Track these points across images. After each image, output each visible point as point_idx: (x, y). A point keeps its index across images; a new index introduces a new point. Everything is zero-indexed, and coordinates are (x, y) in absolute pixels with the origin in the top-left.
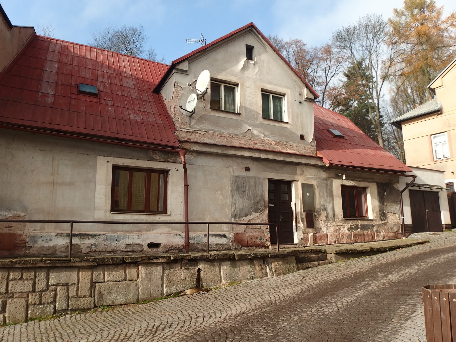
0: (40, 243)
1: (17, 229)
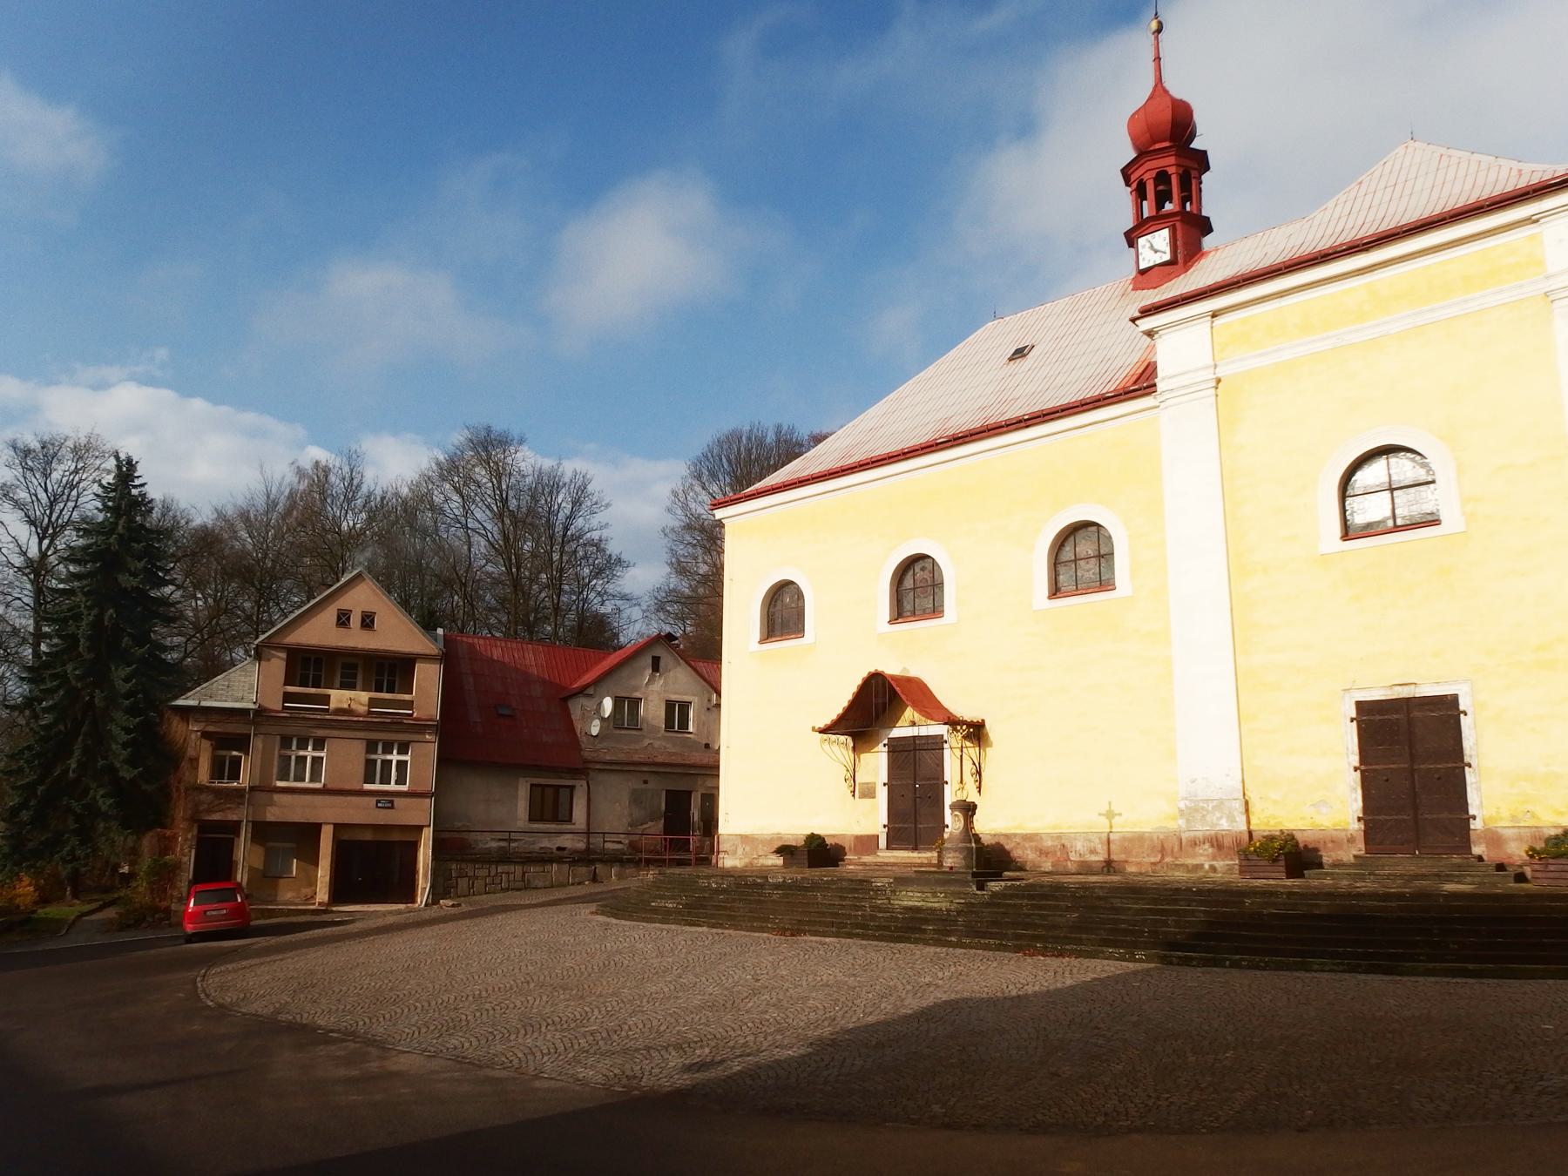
0: (481, 845)
1: (465, 835)
